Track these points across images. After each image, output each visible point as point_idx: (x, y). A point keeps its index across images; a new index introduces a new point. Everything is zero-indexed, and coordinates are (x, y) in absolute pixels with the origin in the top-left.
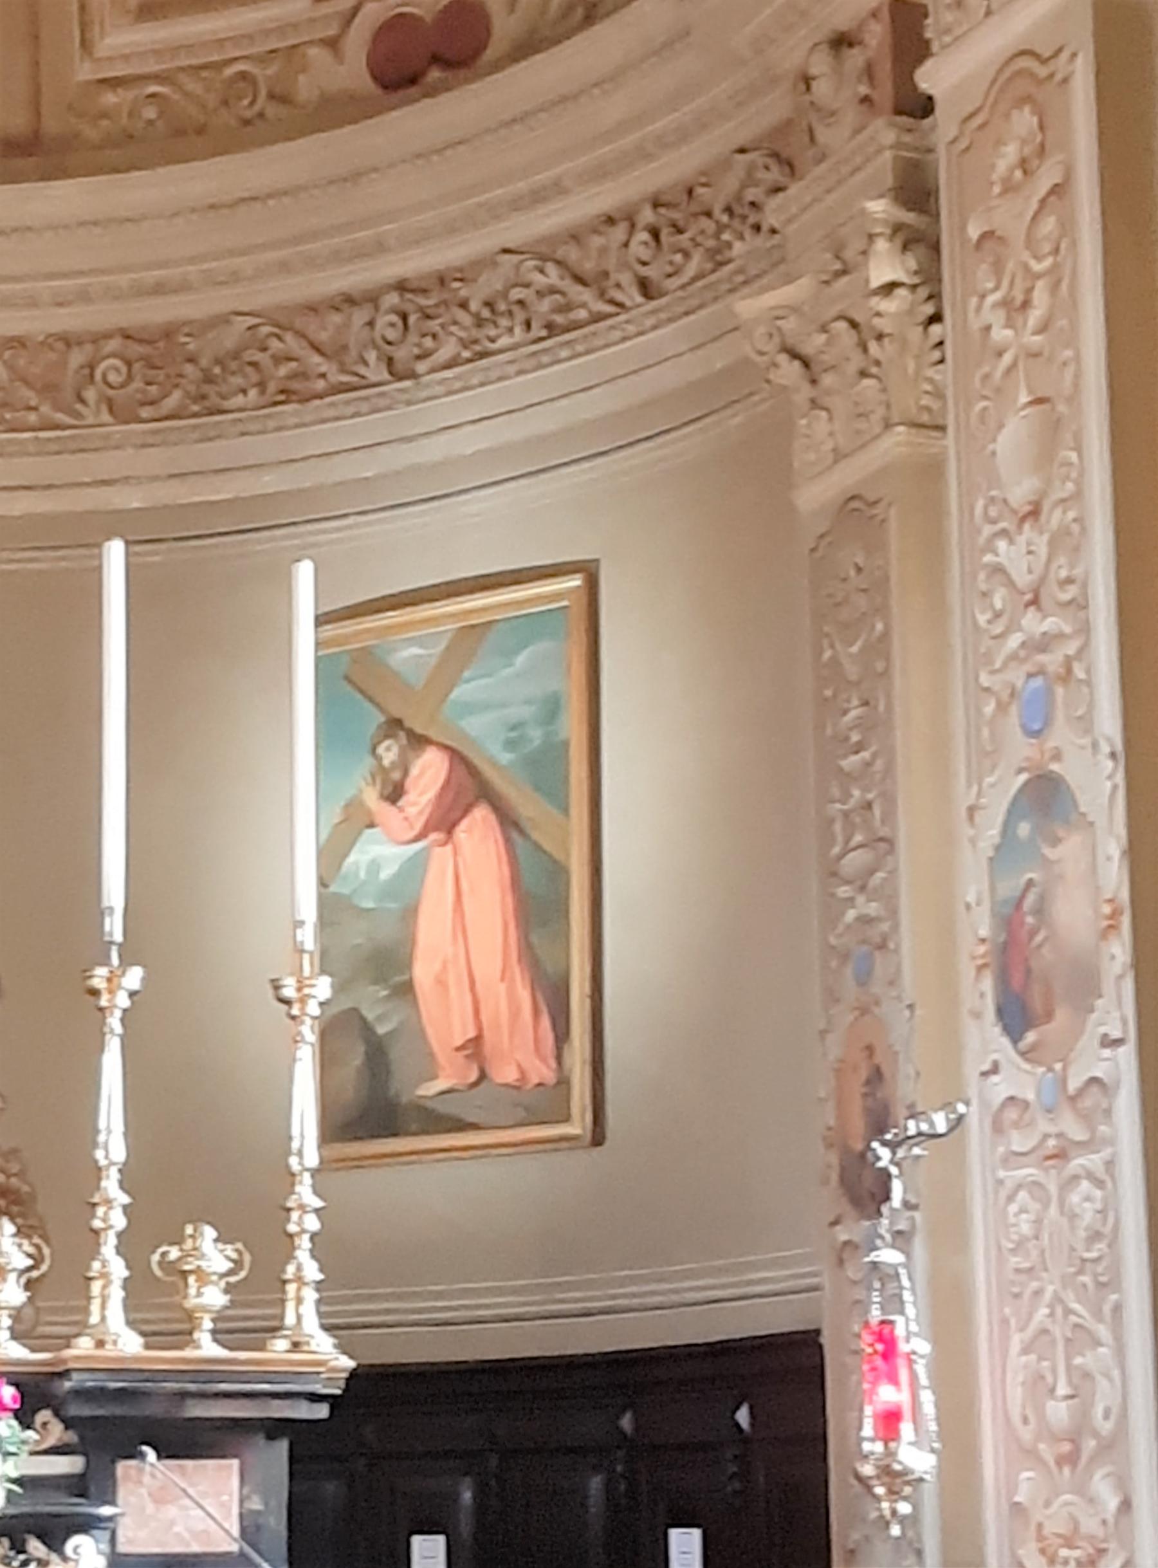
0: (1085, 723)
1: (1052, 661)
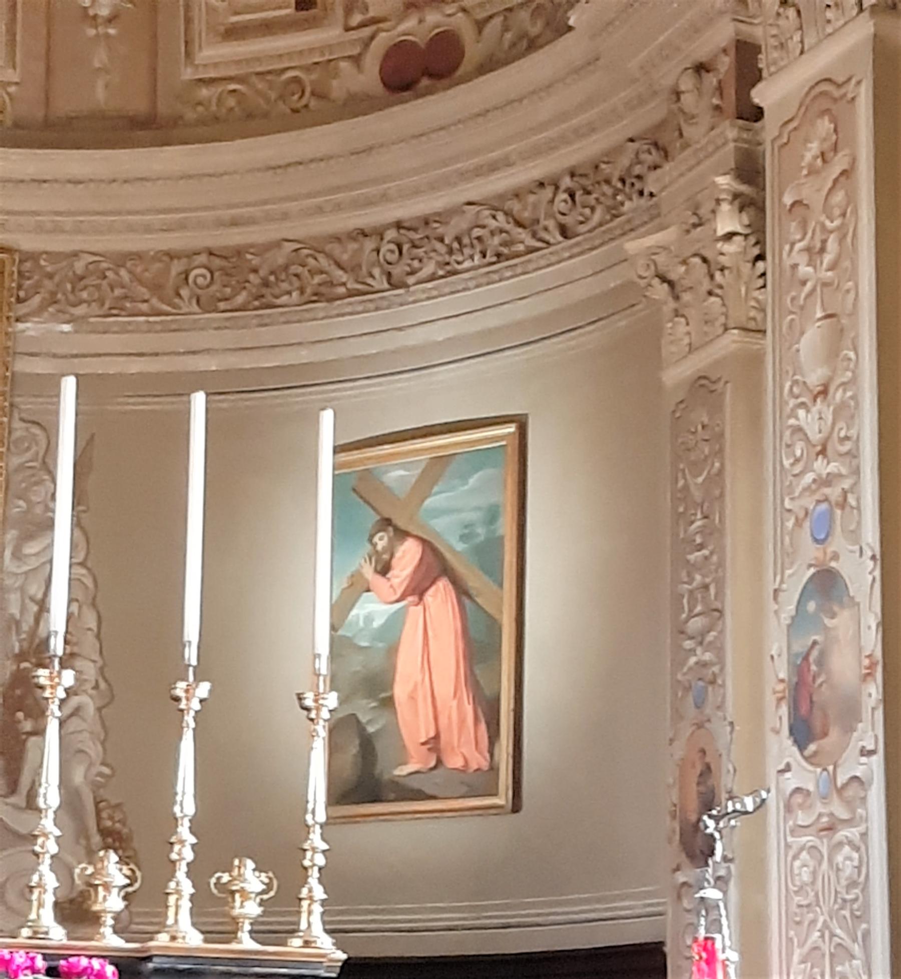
0: (854, 535)
1: (834, 493)
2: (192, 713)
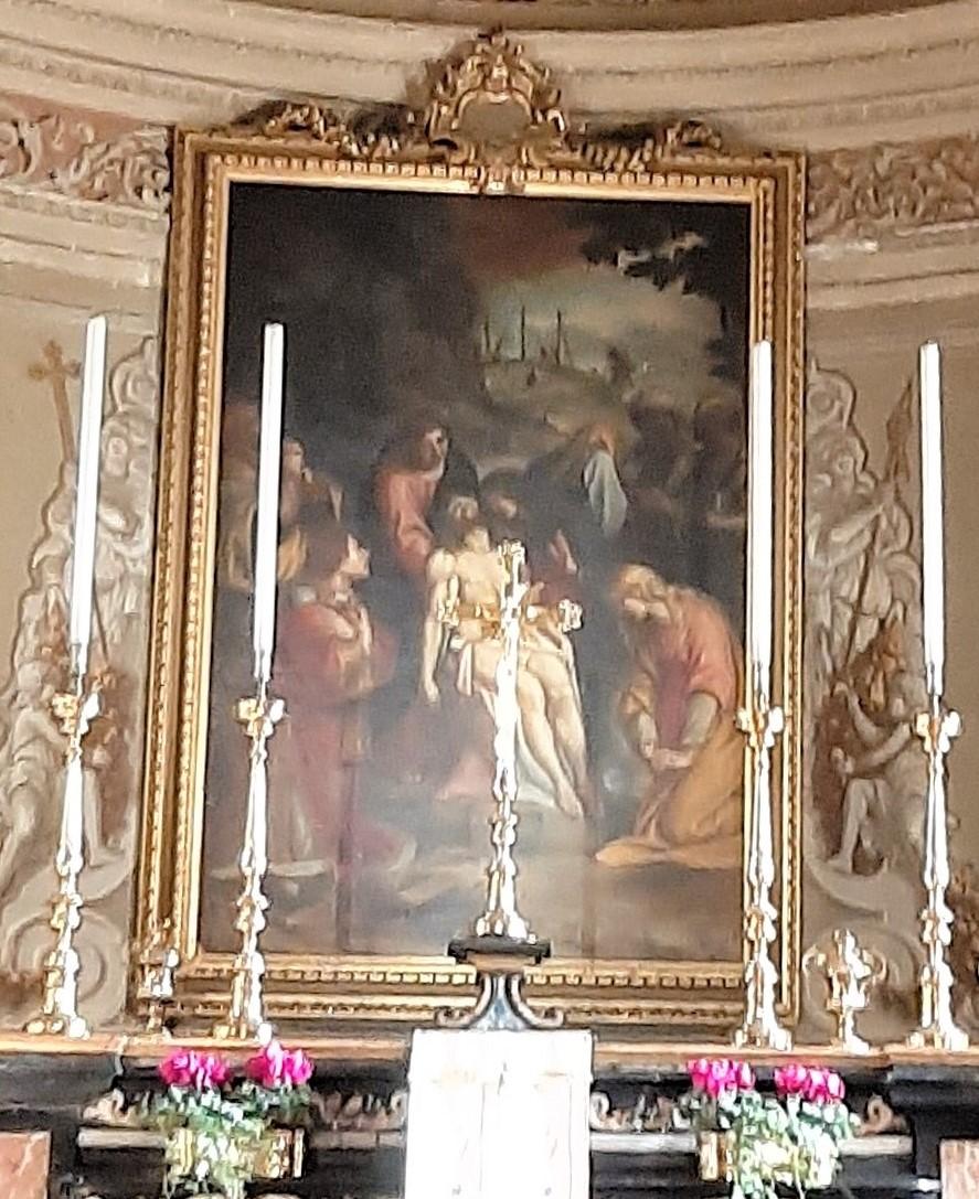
2: (939, 757)
